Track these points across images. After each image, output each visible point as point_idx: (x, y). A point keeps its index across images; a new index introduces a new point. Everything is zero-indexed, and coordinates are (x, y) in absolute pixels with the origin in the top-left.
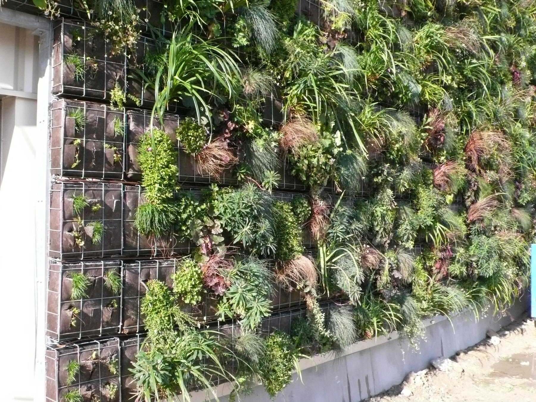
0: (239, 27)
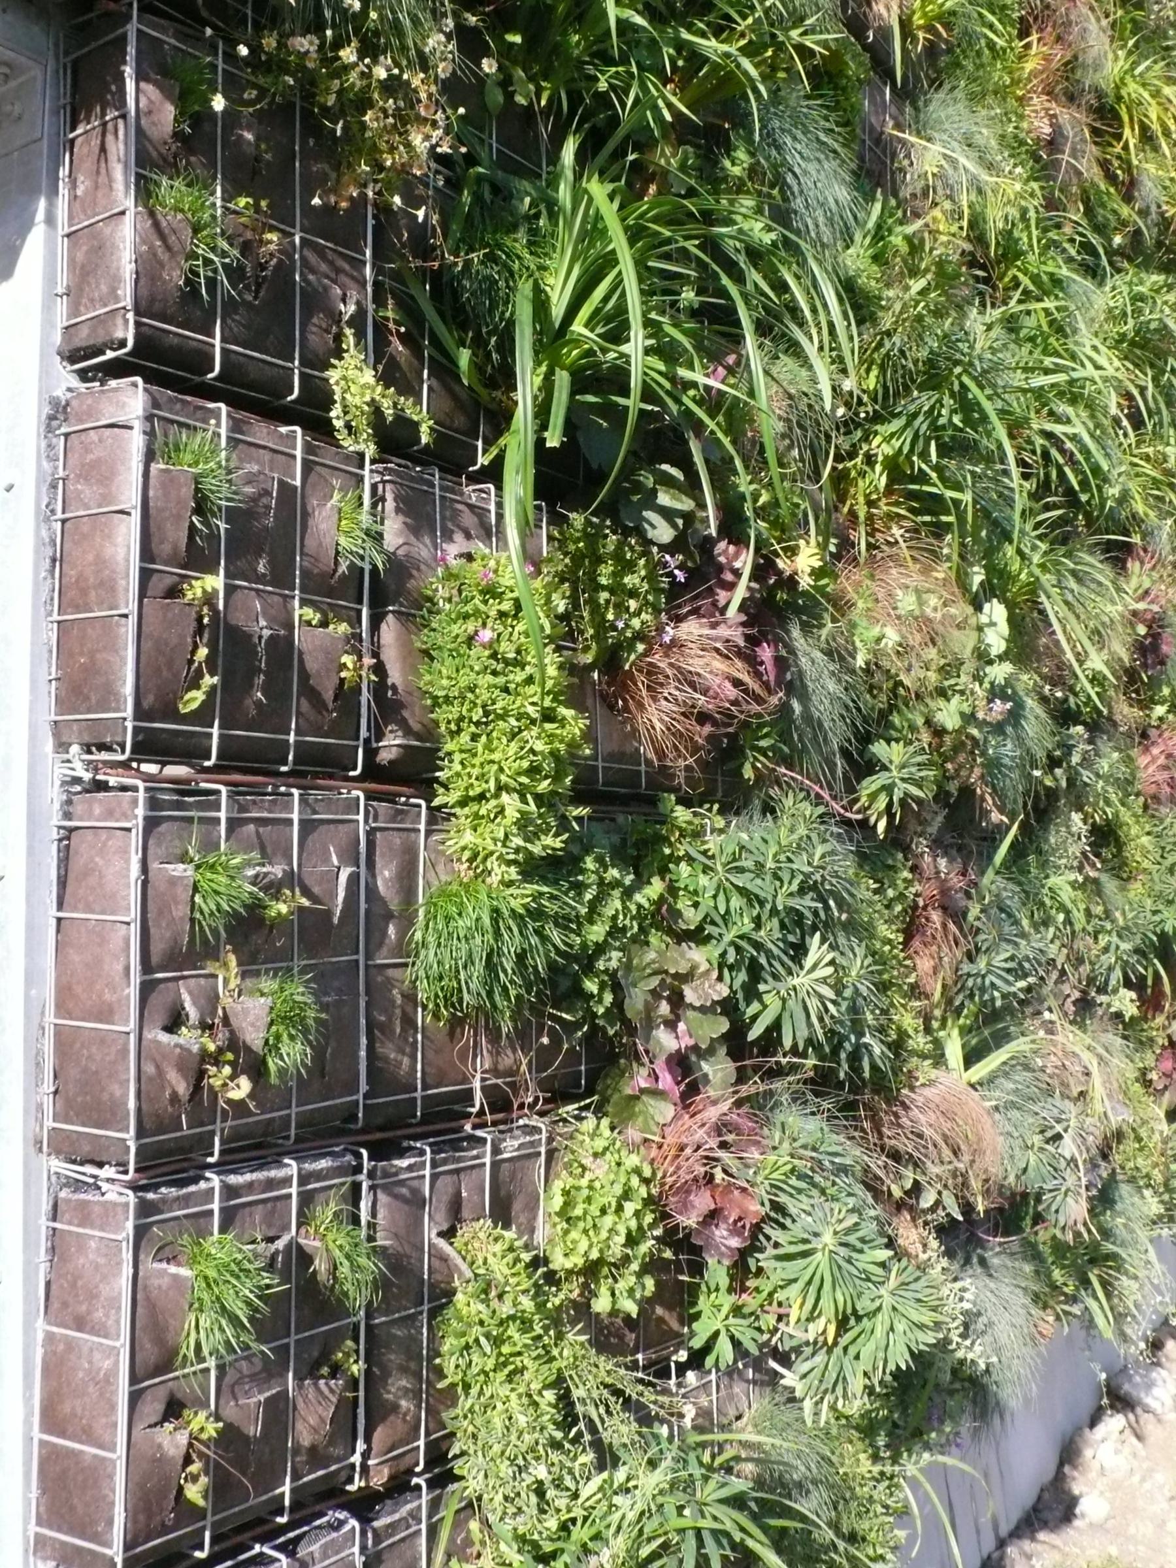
0: (736, 171)
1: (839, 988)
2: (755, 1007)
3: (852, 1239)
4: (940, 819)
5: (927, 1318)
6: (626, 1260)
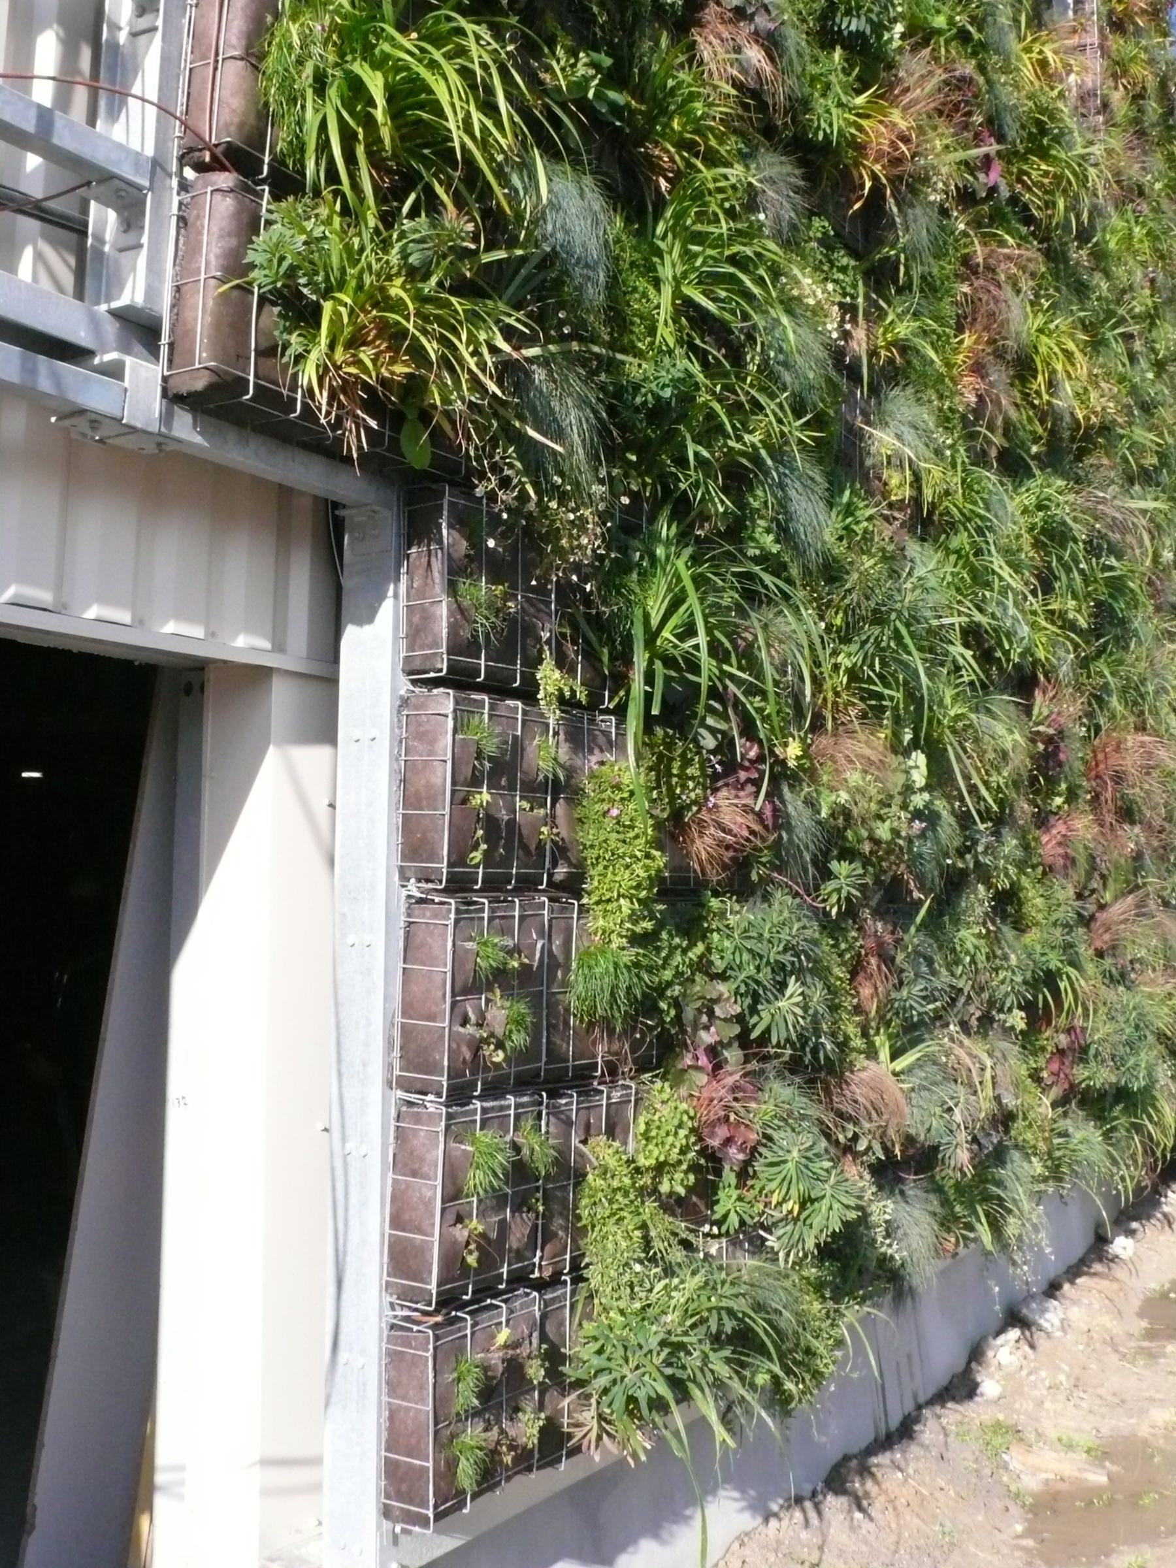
1: (805, 1009)
2: (755, 1019)
3: (810, 1154)
4: (878, 896)
5: (852, 1202)
6: (680, 1162)
